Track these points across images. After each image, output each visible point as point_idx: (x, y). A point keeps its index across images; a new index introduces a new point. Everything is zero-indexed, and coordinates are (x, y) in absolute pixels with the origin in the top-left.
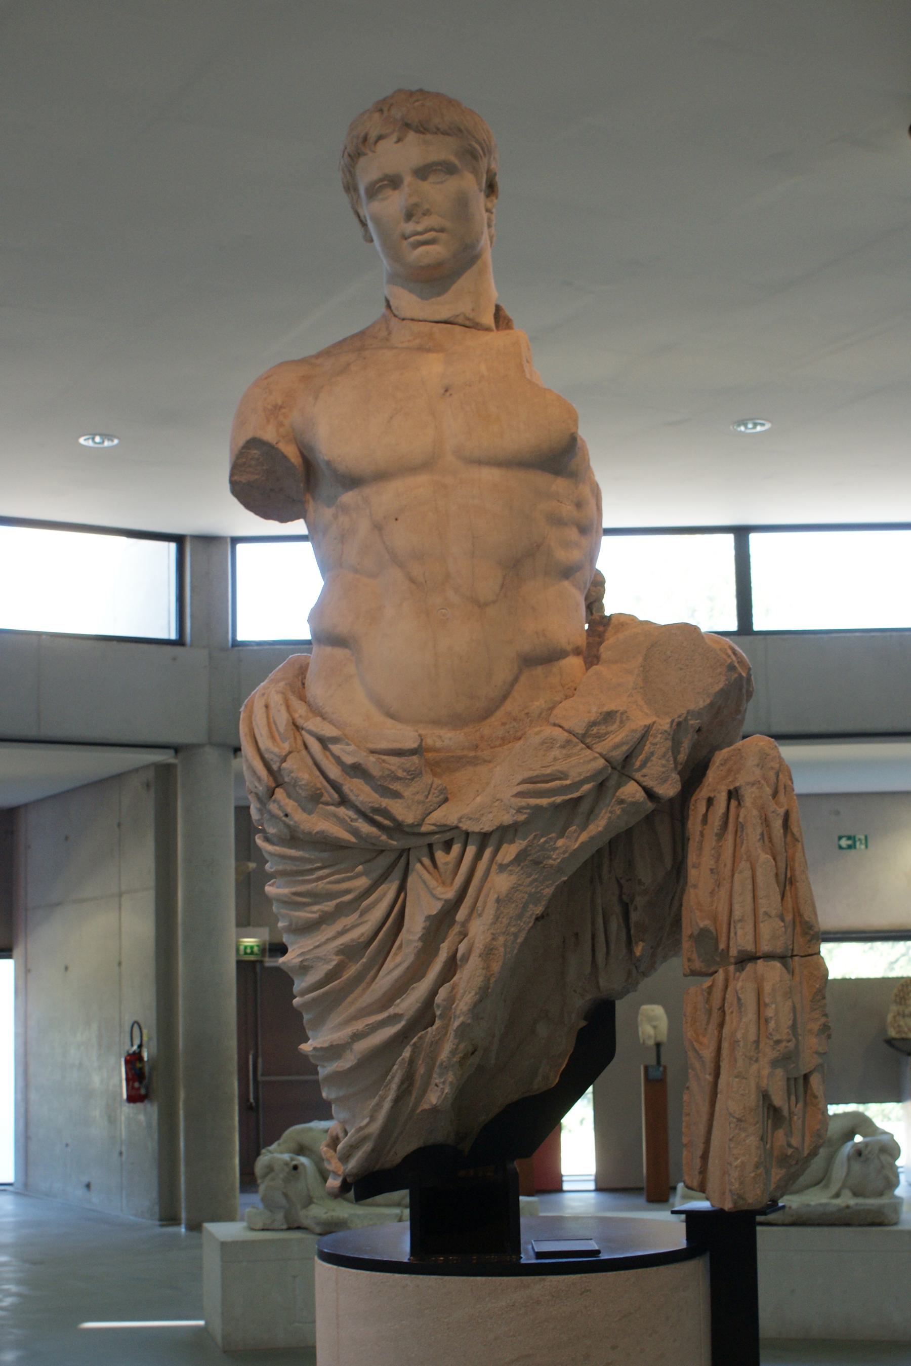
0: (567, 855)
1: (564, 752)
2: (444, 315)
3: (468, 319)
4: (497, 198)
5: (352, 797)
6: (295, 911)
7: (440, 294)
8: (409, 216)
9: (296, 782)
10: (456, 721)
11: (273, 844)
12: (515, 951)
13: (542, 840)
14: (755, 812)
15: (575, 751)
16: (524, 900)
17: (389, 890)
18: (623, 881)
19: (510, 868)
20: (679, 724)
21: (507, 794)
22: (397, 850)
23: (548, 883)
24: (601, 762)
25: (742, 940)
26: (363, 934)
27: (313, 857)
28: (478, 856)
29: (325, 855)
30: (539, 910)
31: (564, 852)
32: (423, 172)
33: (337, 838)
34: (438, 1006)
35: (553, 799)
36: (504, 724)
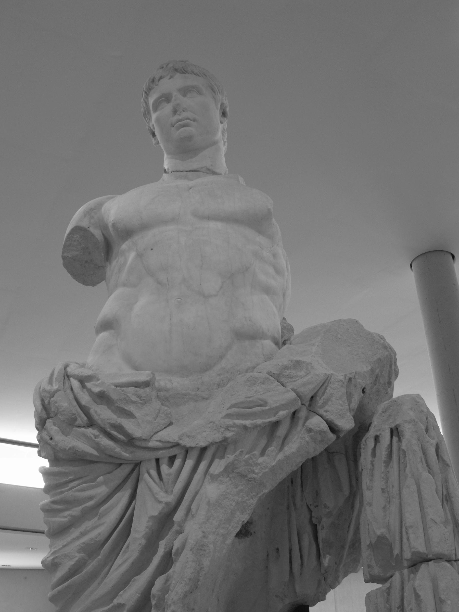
0: (267, 470)
10: (183, 370)
12: (224, 551)
13: (247, 456)
14: (414, 441)
17: (122, 498)
18: (312, 508)
19: (220, 478)
24: (293, 395)
25: (418, 544)
26: (99, 534)
27: (67, 471)
32: (185, 91)
33: (83, 452)
34: (154, 596)
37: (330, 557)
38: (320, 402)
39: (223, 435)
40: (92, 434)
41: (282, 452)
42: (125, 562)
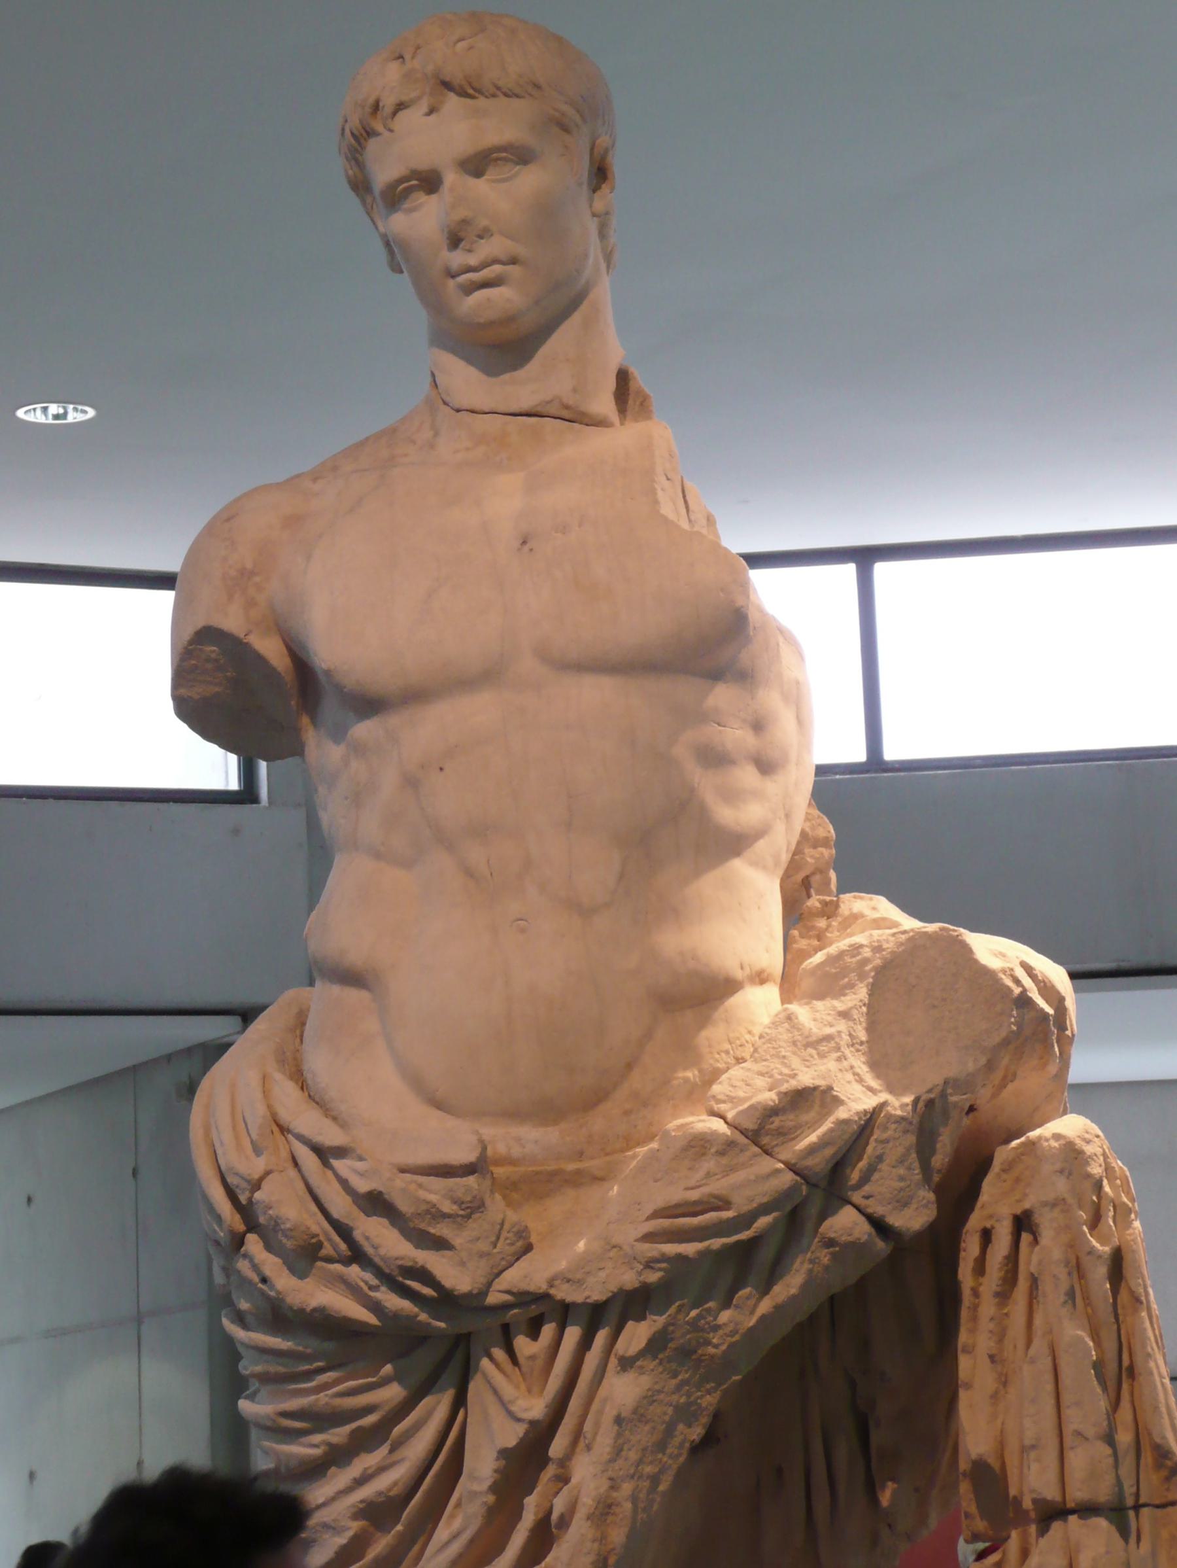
0: (737, 1337)
1: (724, 1161)
2: (527, 398)
3: (567, 407)
4: (612, 190)
5: (369, 1250)
6: (286, 1443)
7: (514, 368)
8: (455, 241)
9: (277, 1224)
10: (546, 1111)
11: (245, 1326)
12: (656, 1507)
13: (693, 1313)
15: (742, 1158)
16: (667, 1418)
19: (639, 1363)
20: (930, 1103)
21: (629, 1234)
22: (445, 1342)
23: (708, 1386)
24: (789, 1178)
25: (1036, 1480)
26: (395, 1484)
27: (309, 1351)
28: (586, 1343)
29: (329, 1346)
30: (696, 1433)
31: (734, 1332)
32: (477, 164)
35: (706, 1243)
36: (627, 1113)
37: (896, 1486)
38: (855, 1176)
39: (642, 1278)
40: (366, 1283)
41: (768, 1297)
42: (455, 1536)
